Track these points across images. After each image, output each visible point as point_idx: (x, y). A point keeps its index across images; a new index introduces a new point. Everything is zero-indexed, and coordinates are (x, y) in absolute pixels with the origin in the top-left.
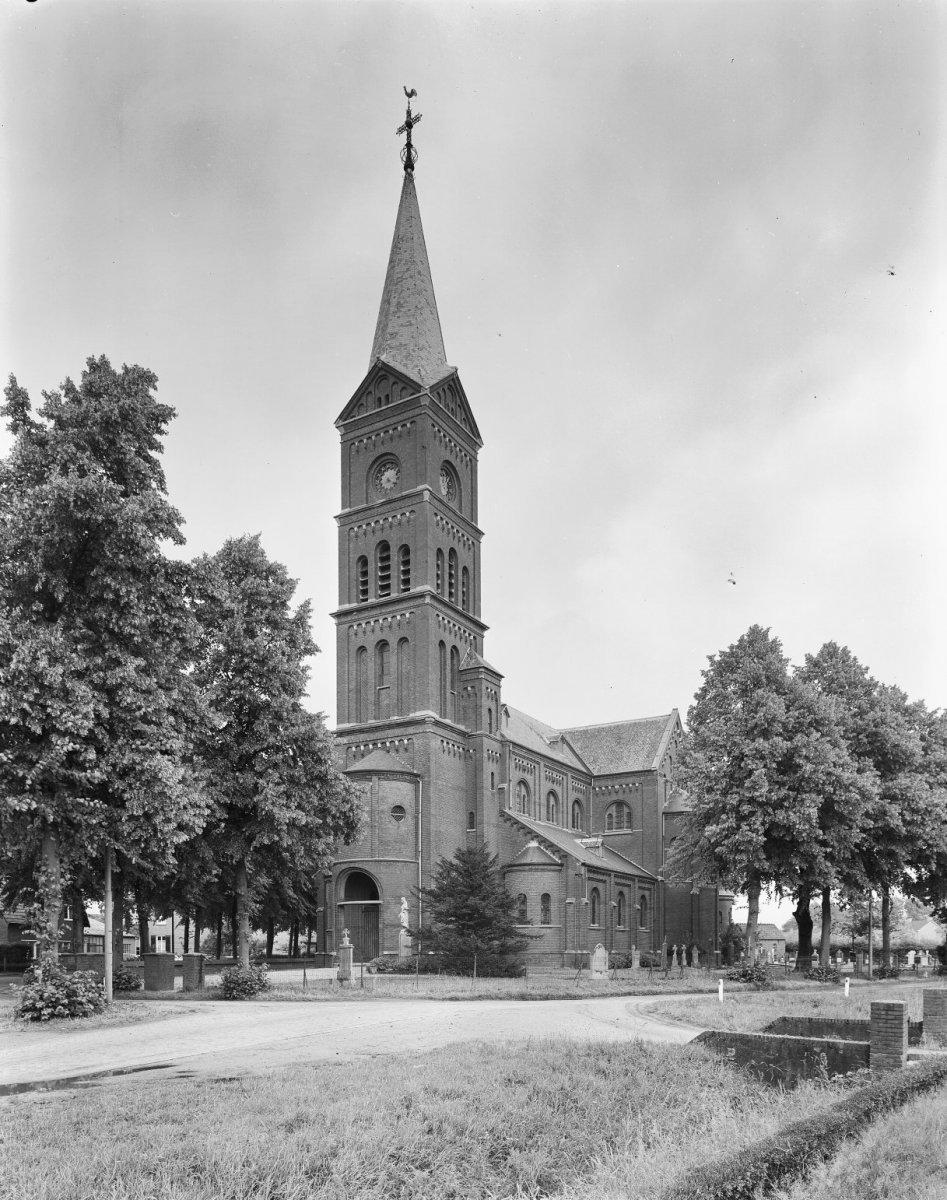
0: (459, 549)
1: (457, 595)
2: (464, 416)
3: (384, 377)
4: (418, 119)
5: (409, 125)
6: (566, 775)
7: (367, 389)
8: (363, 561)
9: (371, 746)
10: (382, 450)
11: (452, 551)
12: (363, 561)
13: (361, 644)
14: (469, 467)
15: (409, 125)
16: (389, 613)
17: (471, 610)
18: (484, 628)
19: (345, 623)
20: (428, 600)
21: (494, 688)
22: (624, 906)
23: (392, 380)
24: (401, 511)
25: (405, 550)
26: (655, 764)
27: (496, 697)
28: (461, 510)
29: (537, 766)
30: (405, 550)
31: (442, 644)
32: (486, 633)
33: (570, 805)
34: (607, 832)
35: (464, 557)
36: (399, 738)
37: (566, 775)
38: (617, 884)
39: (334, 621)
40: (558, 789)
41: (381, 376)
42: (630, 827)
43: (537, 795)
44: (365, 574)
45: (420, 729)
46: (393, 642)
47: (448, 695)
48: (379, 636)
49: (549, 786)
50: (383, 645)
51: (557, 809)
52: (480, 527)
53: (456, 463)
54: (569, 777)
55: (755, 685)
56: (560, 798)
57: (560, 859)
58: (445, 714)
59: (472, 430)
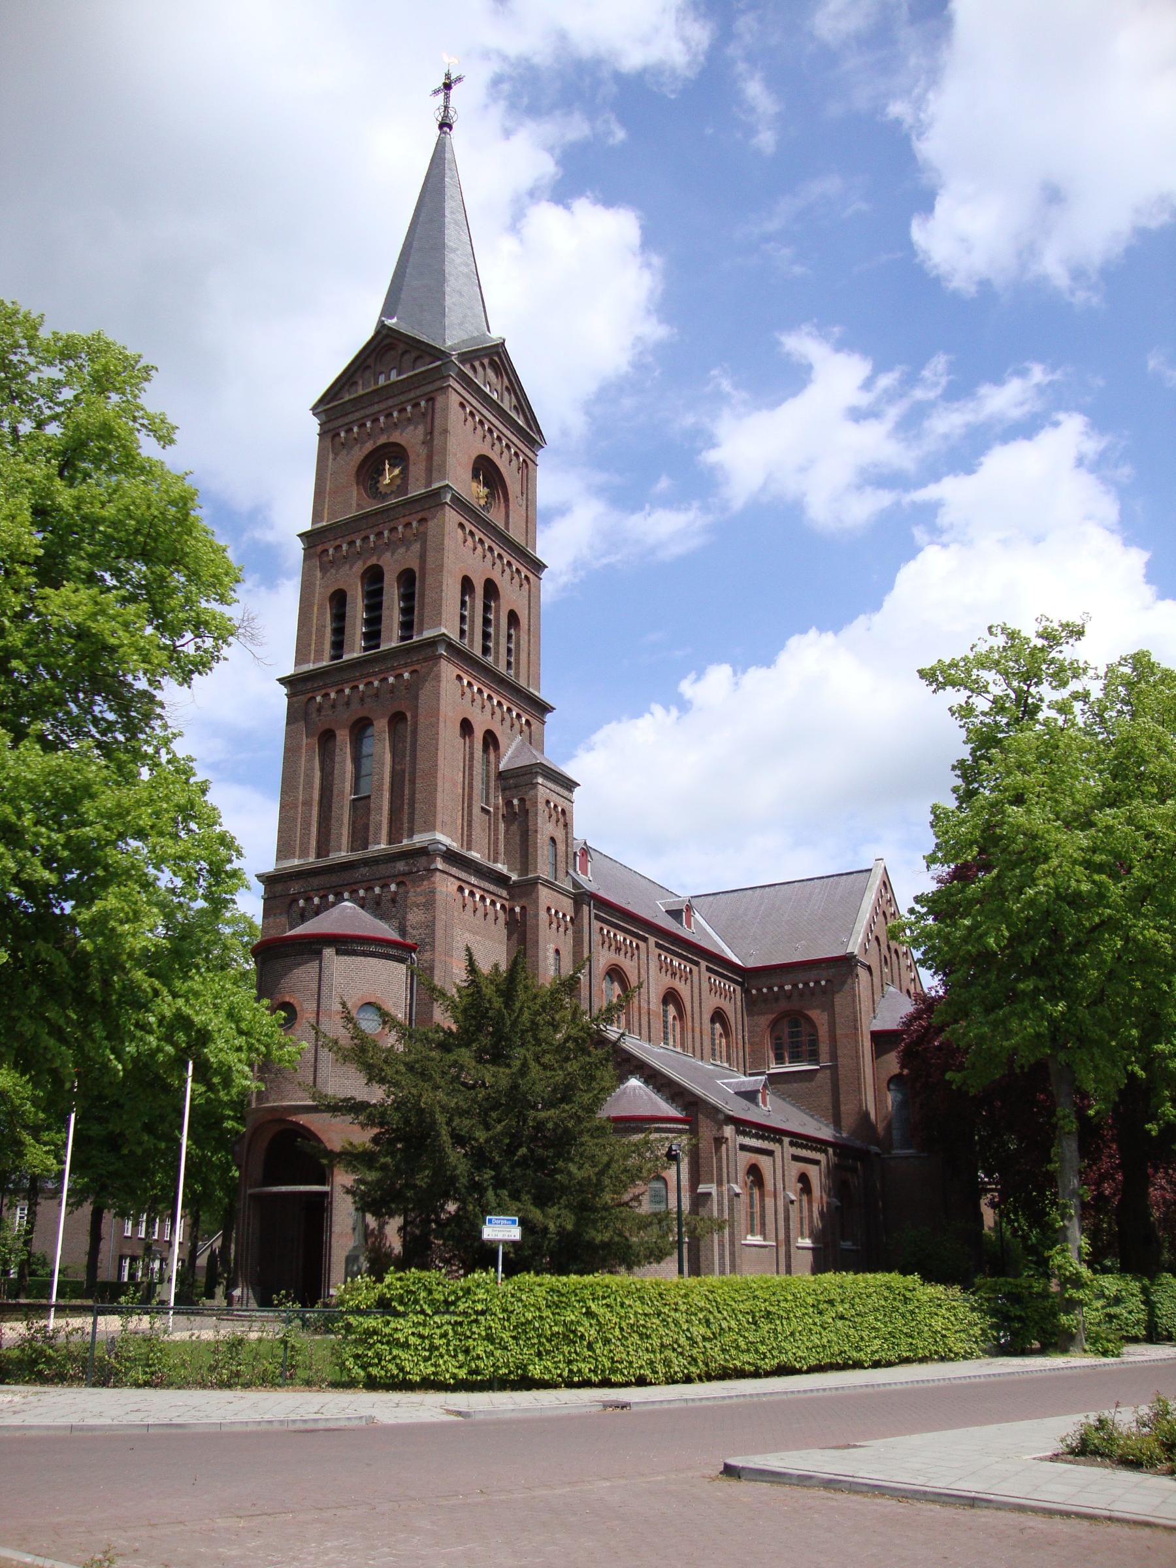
1: (497, 652)
3: (390, 347)
5: (447, 87)
8: (339, 600)
9: (331, 898)
10: (382, 440)
11: (491, 589)
12: (339, 600)
13: (327, 727)
14: (636, 957)
15: (447, 87)
16: (375, 674)
18: (543, 708)
19: (303, 693)
21: (566, 804)
23: (401, 347)
24: (403, 521)
25: (408, 579)
26: (854, 946)
27: (564, 818)
28: (507, 529)
29: (642, 944)
30: (408, 579)
31: (466, 727)
32: (548, 717)
33: (707, 1017)
34: (775, 1069)
35: (511, 596)
38: (795, 1158)
39: (284, 690)
40: (683, 989)
41: (385, 346)
47: (476, 811)
49: (667, 981)
53: (501, 463)
54: (703, 968)
55: (211, 893)
58: (469, 842)
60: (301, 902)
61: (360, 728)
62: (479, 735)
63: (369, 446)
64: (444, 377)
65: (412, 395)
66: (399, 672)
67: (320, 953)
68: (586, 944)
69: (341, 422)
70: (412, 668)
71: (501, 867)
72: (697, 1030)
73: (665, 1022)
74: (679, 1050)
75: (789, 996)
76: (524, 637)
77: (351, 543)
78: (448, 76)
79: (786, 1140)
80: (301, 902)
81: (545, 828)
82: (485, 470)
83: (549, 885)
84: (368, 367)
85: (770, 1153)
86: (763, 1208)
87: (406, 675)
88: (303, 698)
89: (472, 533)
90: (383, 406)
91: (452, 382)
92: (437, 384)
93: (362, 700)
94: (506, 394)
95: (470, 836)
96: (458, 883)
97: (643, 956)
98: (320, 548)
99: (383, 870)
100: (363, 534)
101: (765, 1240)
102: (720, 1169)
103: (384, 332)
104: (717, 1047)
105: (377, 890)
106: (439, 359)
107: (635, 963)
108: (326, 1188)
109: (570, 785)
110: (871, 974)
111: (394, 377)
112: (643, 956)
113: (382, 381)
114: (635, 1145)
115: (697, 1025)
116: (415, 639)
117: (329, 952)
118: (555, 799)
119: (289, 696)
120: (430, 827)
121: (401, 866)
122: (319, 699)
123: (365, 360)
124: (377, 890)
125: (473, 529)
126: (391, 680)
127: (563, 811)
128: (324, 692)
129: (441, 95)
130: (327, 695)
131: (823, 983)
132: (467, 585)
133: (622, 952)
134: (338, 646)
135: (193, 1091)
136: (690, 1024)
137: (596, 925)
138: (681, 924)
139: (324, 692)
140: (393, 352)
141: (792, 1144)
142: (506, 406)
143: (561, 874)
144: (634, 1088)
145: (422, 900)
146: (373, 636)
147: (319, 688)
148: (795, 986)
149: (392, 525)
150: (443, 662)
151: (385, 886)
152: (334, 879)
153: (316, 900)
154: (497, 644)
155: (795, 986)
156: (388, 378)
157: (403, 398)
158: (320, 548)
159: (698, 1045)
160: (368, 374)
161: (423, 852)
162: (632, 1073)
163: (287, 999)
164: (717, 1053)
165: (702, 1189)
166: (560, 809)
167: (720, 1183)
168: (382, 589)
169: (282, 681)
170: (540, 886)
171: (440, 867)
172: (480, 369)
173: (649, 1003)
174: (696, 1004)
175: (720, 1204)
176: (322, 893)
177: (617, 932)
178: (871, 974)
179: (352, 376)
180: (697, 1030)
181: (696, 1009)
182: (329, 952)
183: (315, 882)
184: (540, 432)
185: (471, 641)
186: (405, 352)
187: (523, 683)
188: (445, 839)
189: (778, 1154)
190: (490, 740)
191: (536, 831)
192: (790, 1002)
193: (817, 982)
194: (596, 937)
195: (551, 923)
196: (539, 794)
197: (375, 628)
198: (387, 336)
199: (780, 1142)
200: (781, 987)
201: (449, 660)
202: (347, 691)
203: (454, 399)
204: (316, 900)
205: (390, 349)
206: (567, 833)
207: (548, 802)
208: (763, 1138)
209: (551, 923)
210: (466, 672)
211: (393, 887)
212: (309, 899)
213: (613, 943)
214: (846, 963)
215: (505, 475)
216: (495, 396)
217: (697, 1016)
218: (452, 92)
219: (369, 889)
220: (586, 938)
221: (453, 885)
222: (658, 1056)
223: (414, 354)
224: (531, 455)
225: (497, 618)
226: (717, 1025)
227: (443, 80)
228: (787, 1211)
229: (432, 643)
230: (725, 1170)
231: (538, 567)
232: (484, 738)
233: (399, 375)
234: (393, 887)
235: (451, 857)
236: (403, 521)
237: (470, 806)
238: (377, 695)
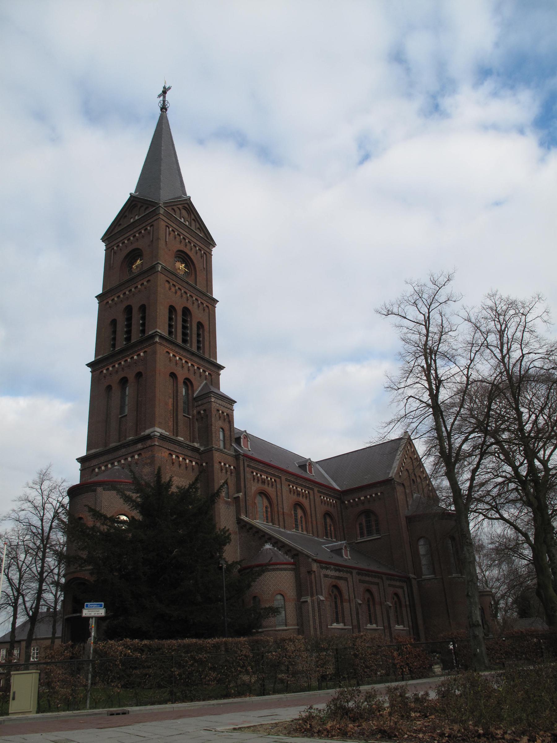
0: (194, 309)
2: (198, 226)
4: (169, 88)
5: (164, 92)
6: (312, 489)
7: (124, 213)
8: (114, 323)
11: (186, 311)
12: (114, 323)
14: (274, 486)
15: (164, 92)
16: (128, 356)
17: (207, 350)
18: (221, 368)
20: (157, 339)
22: (374, 604)
24: (140, 283)
26: (392, 473)
27: (229, 419)
30: (143, 308)
31: (173, 375)
32: (222, 372)
33: (319, 516)
35: (197, 315)
36: (124, 457)
37: (312, 489)
39: (89, 369)
42: (378, 531)
43: (280, 506)
44: (114, 332)
45: (149, 443)
46: (131, 377)
47: (180, 417)
48: (121, 375)
49: (295, 497)
50: (124, 381)
51: (305, 518)
52: (214, 296)
53: (192, 254)
56: (309, 511)
57: (293, 558)
59: (205, 234)
61: (124, 381)
62: (181, 380)
64: (157, 215)
66: (138, 353)
67: (95, 491)
68: (242, 480)
69: (114, 243)
70: (144, 350)
71: (196, 445)
72: (314, 522)
73: (296, 520)
74: (305, 533)
75: (363, 503)
76: (206, 334)
77: (119, 297)
79: (354, 572)
80: (97, 470)
81: (217, 424)
84: (126, 216)
85: (346, 579)
86: (343, 608)
88: (98, 372)
89: (174, 286)
91: (161, 217)
92: (155, 218)
93: (123, 369)
94: (193, 222)
95: (177, 429)
96: (168, 452)
97: (279, 486)
98: (105, 302)
99: (131, 449)
101: (345, 625)
102: (312, 588)
103: (132, 199)
104: (329, 531)
105: (129, 459)
106: (155, 206)
107: (274, 489)
110: (405, 488)
111: (137, 218)
112: (279, 486)
113: (132, 220)
114: (490, 661)
115: (314, 519)
117: (99, 489)
120: (153, 426)
121: (140, 446)
123: (124, 213)
124: (129, 459)
127: (227, 414)
128: (106, 368)
130: (108, 369)
131: (379, 494)
132: (172, 309)
133: (301, 496)
134: (114, 346)
136: (310, 520)
137: (247, 469)
138: (306, 471)
139: (106, 368)
141: (358, 574)
142: (193, 228)
143: (228, 446)
144: (267, 549)
145: (149, 461)
146: (128, 339)
148: (366, 497)
149: (135, 285)
150: (158, 346)
151: (133, 457)
152: (110, 457)
153: (103, 468)
154: (191, 338)
155: (366, 497)
158: (105, 302)
159: (315, 530)
162: (266, 542)
163: (80, 516)
164: (329, 535)
165: (303, 599)
166: (225, 414)
167: (312, 596)
168: (131, 317)
169: (89, 365)
170: (214, 452)
171: (157, 444)
172: (178, 211)
173: (283, 509)
174: (313, 509)
175: (313, 607)
176: (105, 464)
177: (262, 473)
178: (405, 488)
179: (119, 221)
180: (314, 522)
181: (313, 512)
182: (99, 489)
183: (102, 459)
185: (176, 336)
186: (141, 207)
187: (207, 356)
188: (158, 431)
189: (350, 579)
190: (187, 382)
191: (211, 425)
193: (376, 494)
194: (249, 476)
195: (222, 470)
196: (212, 407)
198: (133, 201)
199: (351, 573)
200: (359, 499)
201: (160, 344)
202: (117, 366)
203: (163, 224)
204: (103, 468)
206: (230, 426)
207: (218, 410)
208: (340, 571)
209: (222, 470)
210: (172, 350)
211: (136, 457)
212: (100, 468)
213: (260, 479)
214: (389, 482)
216: (187, 223)
217: (313, 515)
218: (167, 95)
219: (126, 459)
220: (242, 477)
221: (166, 454)
222: (287, 536)
223: (145, 206)
224: (208, 250)
225: (191, 325)
227: (162, 89)
228: (357, 609)
229: (152, 337)
230: (314, 588)
236: (140, 283)
237: (177, 415)
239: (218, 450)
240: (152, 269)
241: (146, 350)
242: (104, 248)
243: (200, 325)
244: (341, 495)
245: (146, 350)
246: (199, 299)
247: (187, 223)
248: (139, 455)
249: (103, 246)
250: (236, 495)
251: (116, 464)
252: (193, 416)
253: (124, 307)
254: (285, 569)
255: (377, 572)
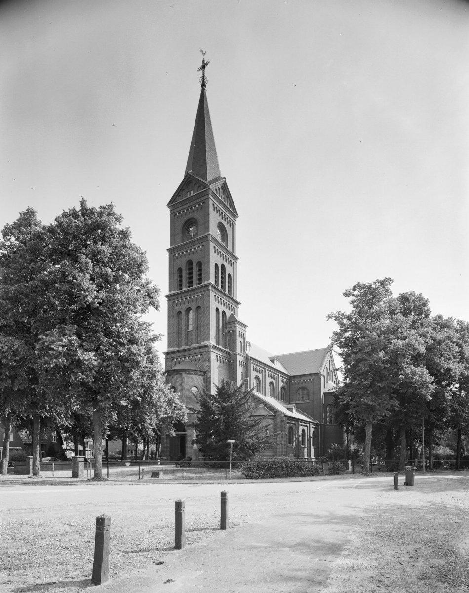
3: (190, 182)
4: (207, 63)
5: (204, 67)
8: (180, 270)
11: (223, 266)
12: (180, 270)
15: (204, 67)
18: (238, 303)
30: (200, 264)
31: (217, 310)
32: (239, 306)
35: (229, 269)
39: (166, 299)
53: (225, 224)
60: (175, 360)
61: (188, 310)
63: (185, 219)
65: (198, 201)
67: (181, 374)
69: (177, 210)
77: (183, 253)
78: (203, 61)
80: (175, 360)
82: (221, 227)
83: (239, 354)
87: (201, 295)
90: (189, 205)
92: (206, 197)
98: (173, 254)
100: (186, 249)
108: (186, 433)
109: (245, 326)
116: (203, 284)
118: (241, 331)
119: (168, 301)
122: (176, 302)
125: (218, 248)
126: (196, 296)
129: (202, 71)
130: (178, 301)
132: (216, 266)
135: (225, 463)
137: (252, 365)
140: (191, 184)
147: (176, 299)
152: (183, 354)
156: (190, 194)
157: (195, 202)
160: (184, 193)
161: (207, 346)
182: (184, 373)
183: (179, 354)
184: (237, 213)
192: (297, 387)
197: (191, 276)
202: (184, 300)
205: (190, 183)
215: (227, 231)
218: (206, 69)
223: (198, 185)
224: (234, 221)
226: (283, 390)
229: (207, 285)
231: (236, 258)
232: (222, 314)
233: (194, 193)
234: (199, 356)
235: (215, 347)
238: (192, 301)
239: (239, 354)
240: (207, 237)
241: (204, 293)
242: (169, 212)
243: (229, 275)
244: (290, 378)
245: (204, 293)
246: (230, 258)
247: (223, 200)
248: (201, 355)
249: (168, 211)
250: (246, 378)
251: (187, 358)
252: (226, 333)
253: (193, 263)
254: (270, 418)
255: (308, 421)
